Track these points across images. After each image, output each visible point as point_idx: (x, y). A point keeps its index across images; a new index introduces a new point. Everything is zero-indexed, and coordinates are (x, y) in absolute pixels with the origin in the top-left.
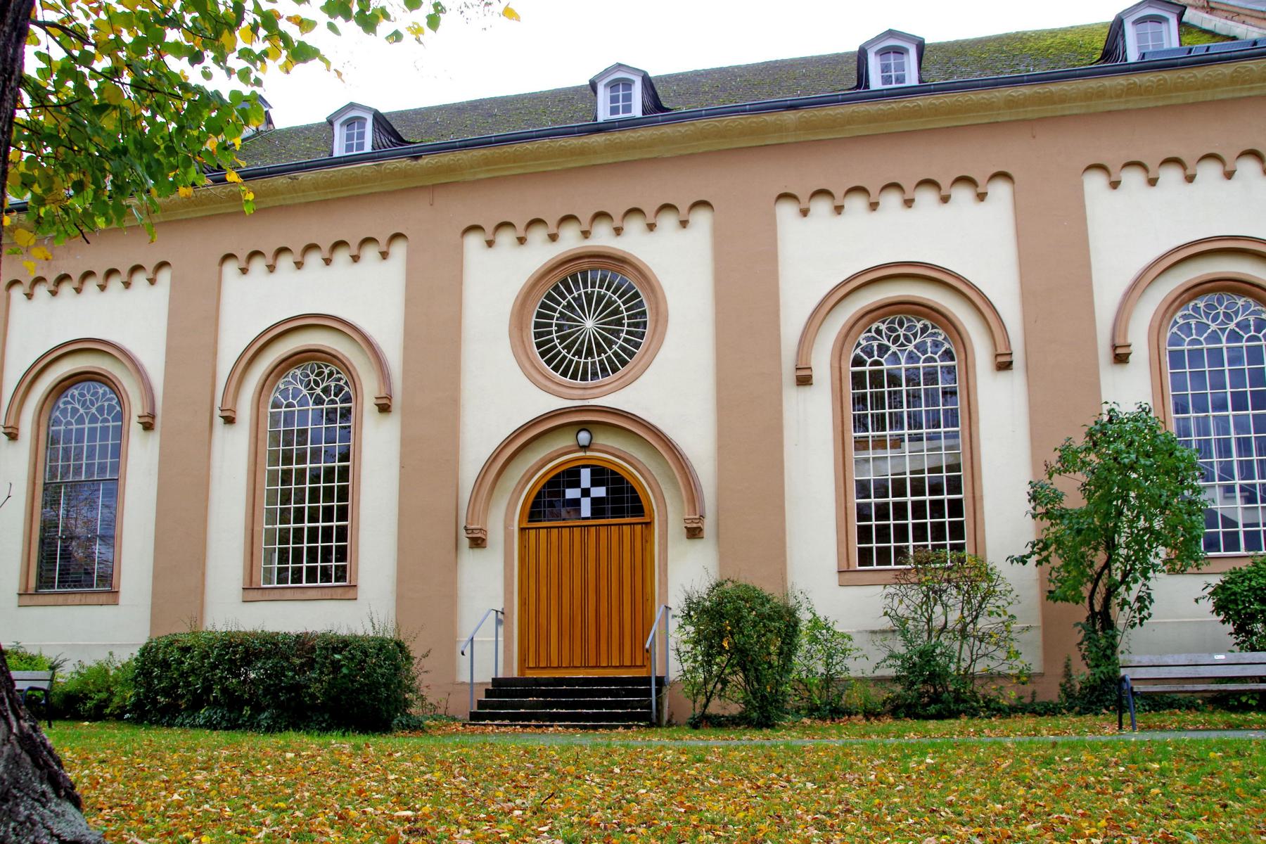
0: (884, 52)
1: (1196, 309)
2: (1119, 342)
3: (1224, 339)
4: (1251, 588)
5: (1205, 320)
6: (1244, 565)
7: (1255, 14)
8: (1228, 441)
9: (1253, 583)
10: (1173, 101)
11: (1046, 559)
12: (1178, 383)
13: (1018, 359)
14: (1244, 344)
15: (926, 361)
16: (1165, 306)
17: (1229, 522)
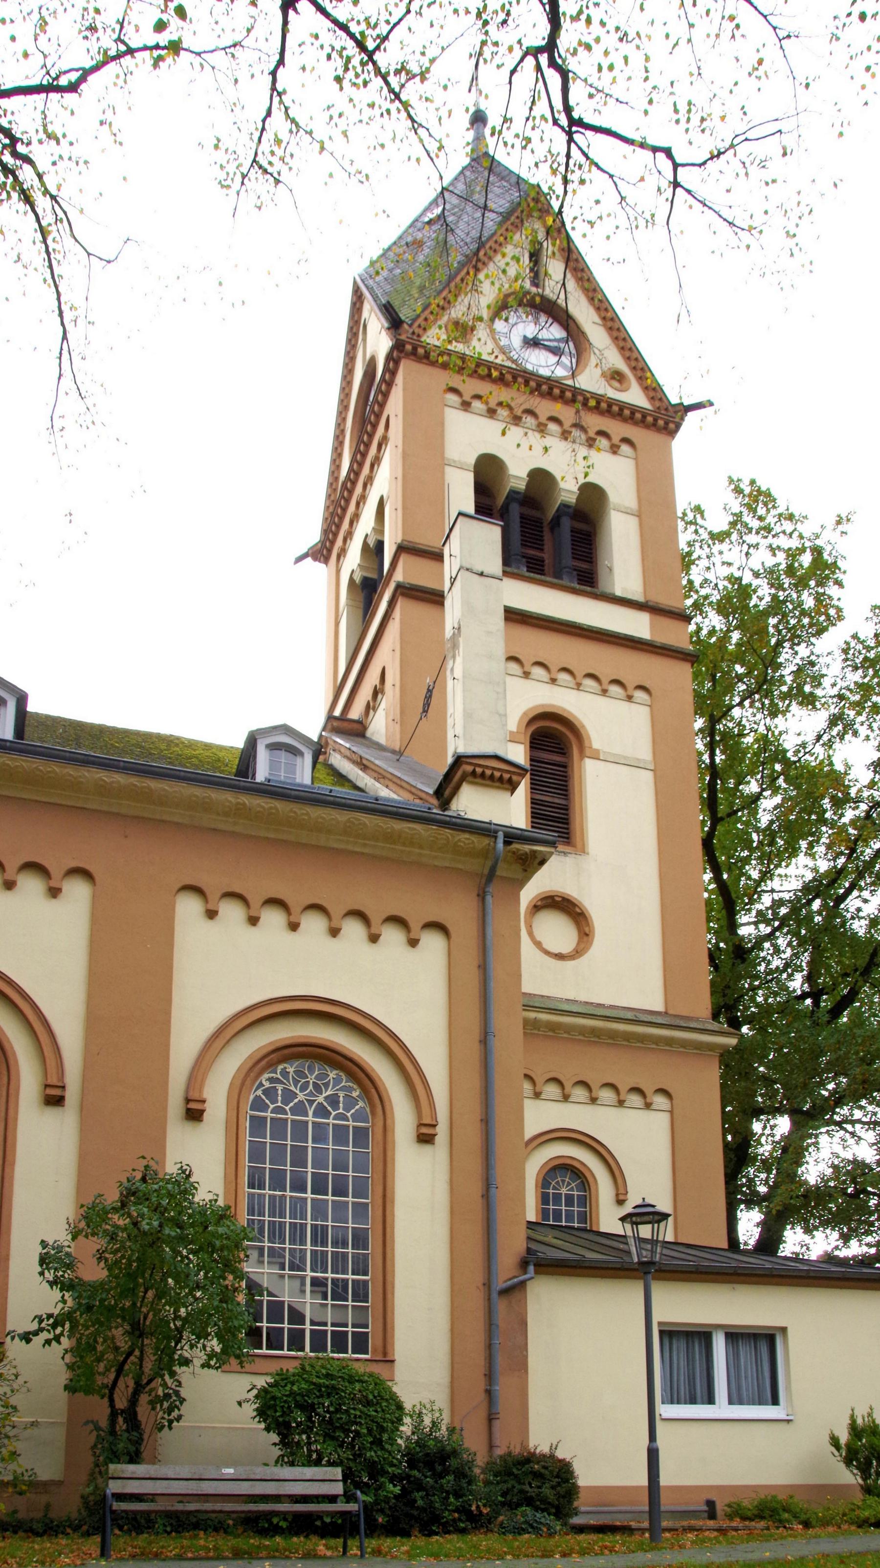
0: (274, 747)
1: (285, 1073)
2: (194, 1095)
3: (311, 1113)
4: (292, 1393)
5: (293, 1088)
6: (292, 1367)
7: (395, 780)
8: (303, 1227)
9: (295, 1388)
10: (284, 837)
11: (57, 1339)
12: (257, 1153)
13: (72, 1095)
14: (331, 1121)
15: (336, 1117)
16: (250, 1064)
17: (297, 1316)
